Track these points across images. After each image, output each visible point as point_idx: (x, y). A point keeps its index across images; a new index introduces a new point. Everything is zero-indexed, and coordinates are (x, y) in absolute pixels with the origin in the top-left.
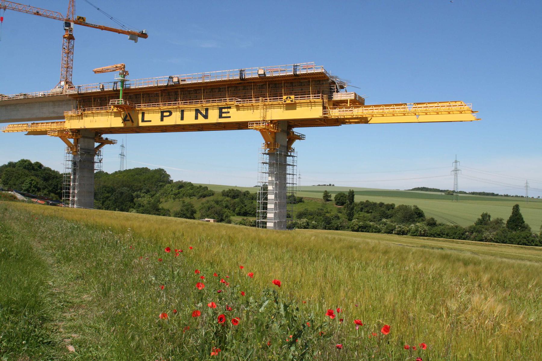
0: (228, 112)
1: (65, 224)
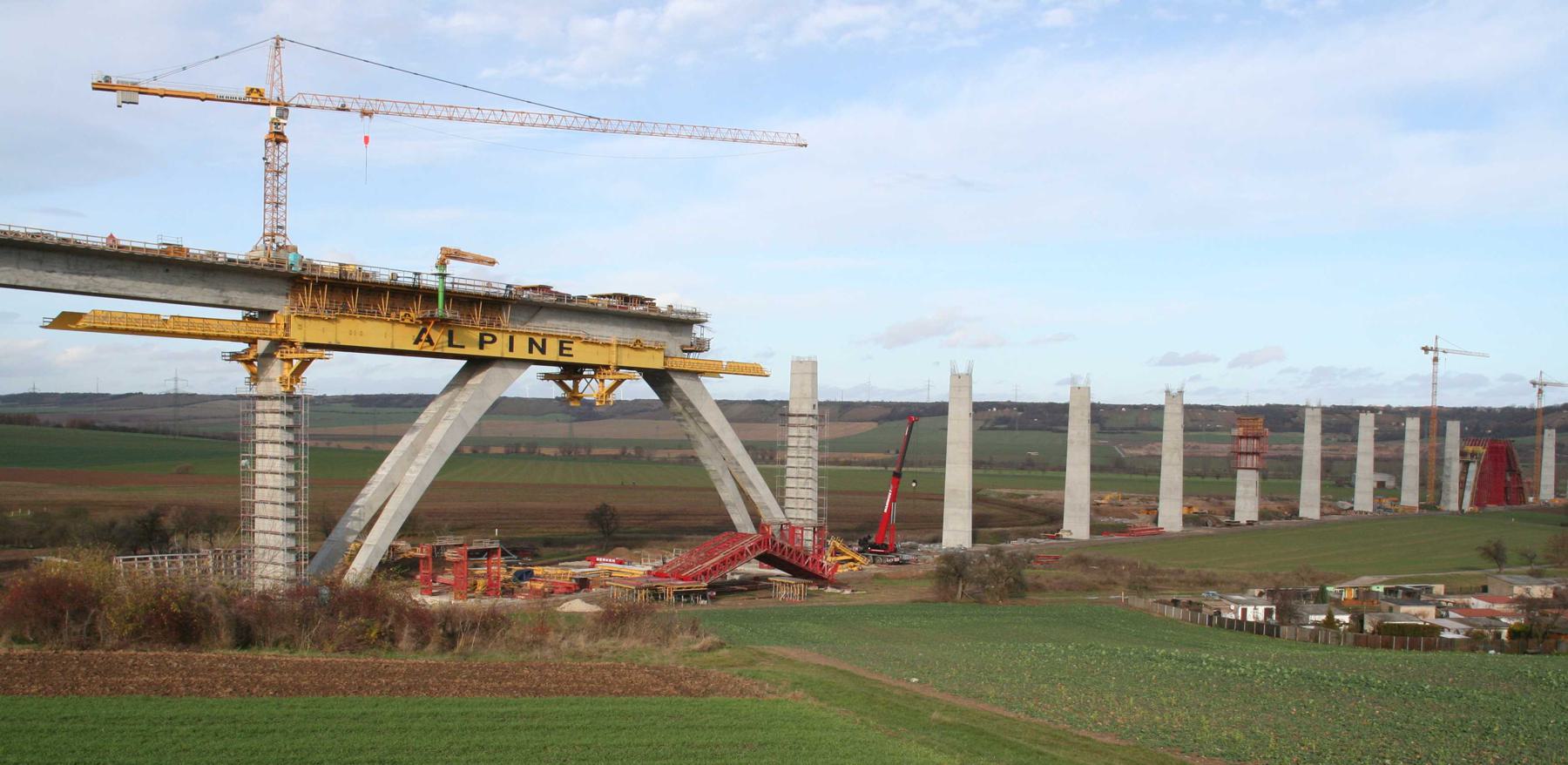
0: (570, 349)
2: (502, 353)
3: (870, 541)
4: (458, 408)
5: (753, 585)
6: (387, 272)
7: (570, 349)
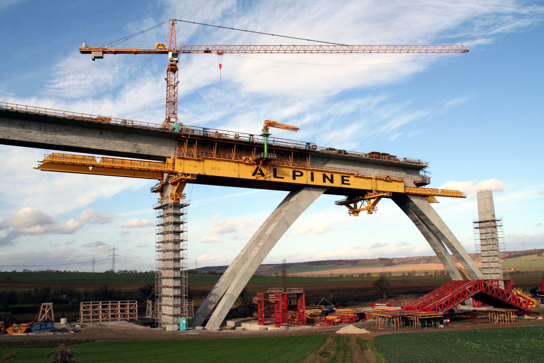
0: (348, 180)
1: (461, 348)
2: (307, 182)
3: (537, 291)
4: (283, 214)
5: (472, 315)
6: (232, 134)
7: (348, 180)
